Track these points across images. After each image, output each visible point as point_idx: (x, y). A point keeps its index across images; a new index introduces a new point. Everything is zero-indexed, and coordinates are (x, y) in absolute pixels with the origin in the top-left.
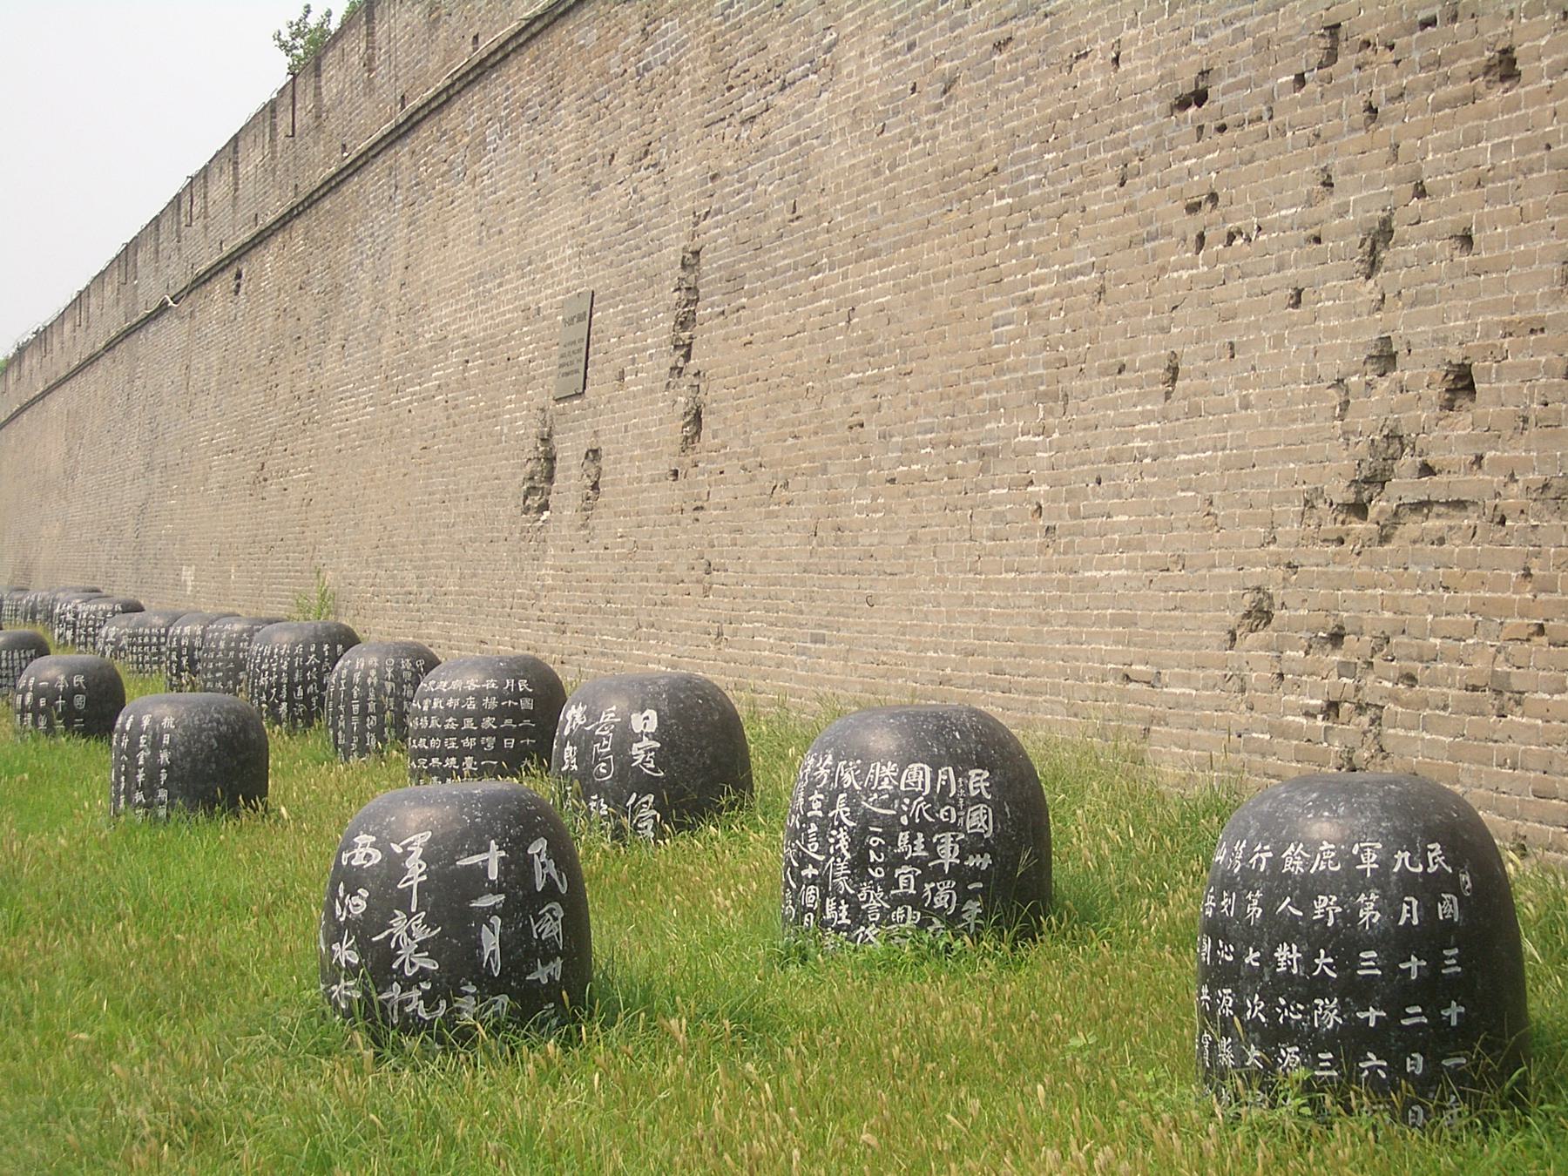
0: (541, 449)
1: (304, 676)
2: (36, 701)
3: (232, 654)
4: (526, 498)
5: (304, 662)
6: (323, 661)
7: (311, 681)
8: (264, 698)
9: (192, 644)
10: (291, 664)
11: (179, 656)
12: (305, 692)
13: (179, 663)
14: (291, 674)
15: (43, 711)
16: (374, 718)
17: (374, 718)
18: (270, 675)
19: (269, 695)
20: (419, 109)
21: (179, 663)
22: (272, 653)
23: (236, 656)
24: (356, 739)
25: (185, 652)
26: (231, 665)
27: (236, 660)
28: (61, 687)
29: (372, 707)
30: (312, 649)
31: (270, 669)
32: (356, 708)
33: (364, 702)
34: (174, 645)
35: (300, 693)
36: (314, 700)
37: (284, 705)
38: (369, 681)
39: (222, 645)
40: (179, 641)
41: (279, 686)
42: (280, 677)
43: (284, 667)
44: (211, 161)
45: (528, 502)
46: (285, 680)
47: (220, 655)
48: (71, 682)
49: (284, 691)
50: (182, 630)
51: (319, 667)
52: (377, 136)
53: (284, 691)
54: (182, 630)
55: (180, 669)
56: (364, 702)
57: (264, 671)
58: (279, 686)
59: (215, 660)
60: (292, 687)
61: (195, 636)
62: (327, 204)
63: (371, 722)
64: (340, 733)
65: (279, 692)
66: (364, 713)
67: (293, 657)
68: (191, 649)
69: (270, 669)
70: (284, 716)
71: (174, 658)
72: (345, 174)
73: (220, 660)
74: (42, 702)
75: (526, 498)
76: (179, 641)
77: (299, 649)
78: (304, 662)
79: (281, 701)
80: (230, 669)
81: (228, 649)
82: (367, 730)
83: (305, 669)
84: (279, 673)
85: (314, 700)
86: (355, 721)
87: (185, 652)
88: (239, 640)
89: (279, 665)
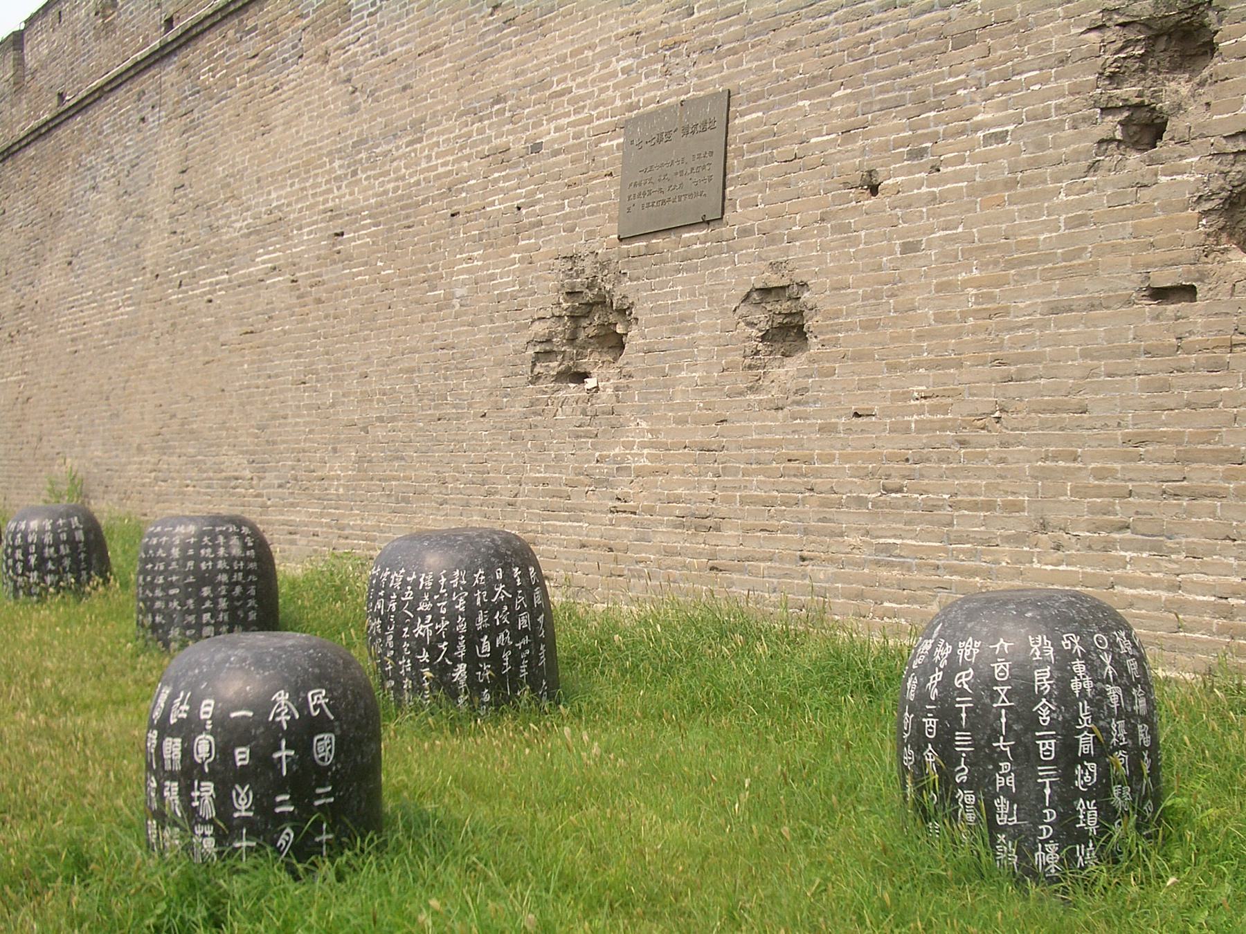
0: (565, 305)
1: (491, 620)
2: (224, 752)
3: (191, 564)
4: (534, 365)
5: (490, 596)
6: (515, 595)
7: (503, 626)
8: (425, 656)
9: (41, 540)
10: (470, 601)
11: (26, 554)
12: (493, 643)
13: (26, 562)
14: (471, 615)
15: (243, 776)
16: (1093, 767)
17: (1093, 767)
18: (436, 620)
19: (434, 651)
20: (86, 97)
21: (26, 562)
22: (436, 586)
23: (197, 566)
24: (1050, 815)
25: (33, 549)
26: (191, 579)
27: (197, 571)
28: (284, 719)
29: (1085, 744)
30: (499, 576)
31: (434, 610)
32: (1047, 746)
33: (1067, 732)
34: (18, 541)
35: (486, 646)
36: (506, 656)
37: (462, 668)
38: (1075, 686)
39: (176, 552)
40: (24, 537)
41: (452, 637)
42: (454, 624)
43: (461, 607)
44: (30, 21)
45: (537, 370)
46: (462, 627)
47: (174, 565)
48: (303, 706)
49: (462, 644)
50: (27, 525)
51: (510, 602)
52: (115, 71)
53: (462, 644)
54: (27, 525)
55: (27, 568)
56: (1067, 732)
57: (423, 615)
58: (452, 637)
59: (166, 573)
60: (473, 638)
61: (45, 532)
62: (31, 152)
63: (1086, 776)
64: (1002, 804)
65: (452, 648)
66: (1068, 756)
67: (471, 589)
68: (40, 546)
69: (434, 610)
70: (463, 684)
71: (19, 555)
72: (64, 117)
73: (173, 572)
74: (242, 756)
75: (534, 365)
76: (24, 537)
77: (479, 577)
78: (490, 596)
79: (457, 661)
80: (190, 584)
81: (186, 558)
82: (1077, 794)
83: (492, 609)
84: (452, 616)
85: (506, 656)
86: (1047, 778)
87: (33, 549)
88: (199, 546)
89: (450, 606)
